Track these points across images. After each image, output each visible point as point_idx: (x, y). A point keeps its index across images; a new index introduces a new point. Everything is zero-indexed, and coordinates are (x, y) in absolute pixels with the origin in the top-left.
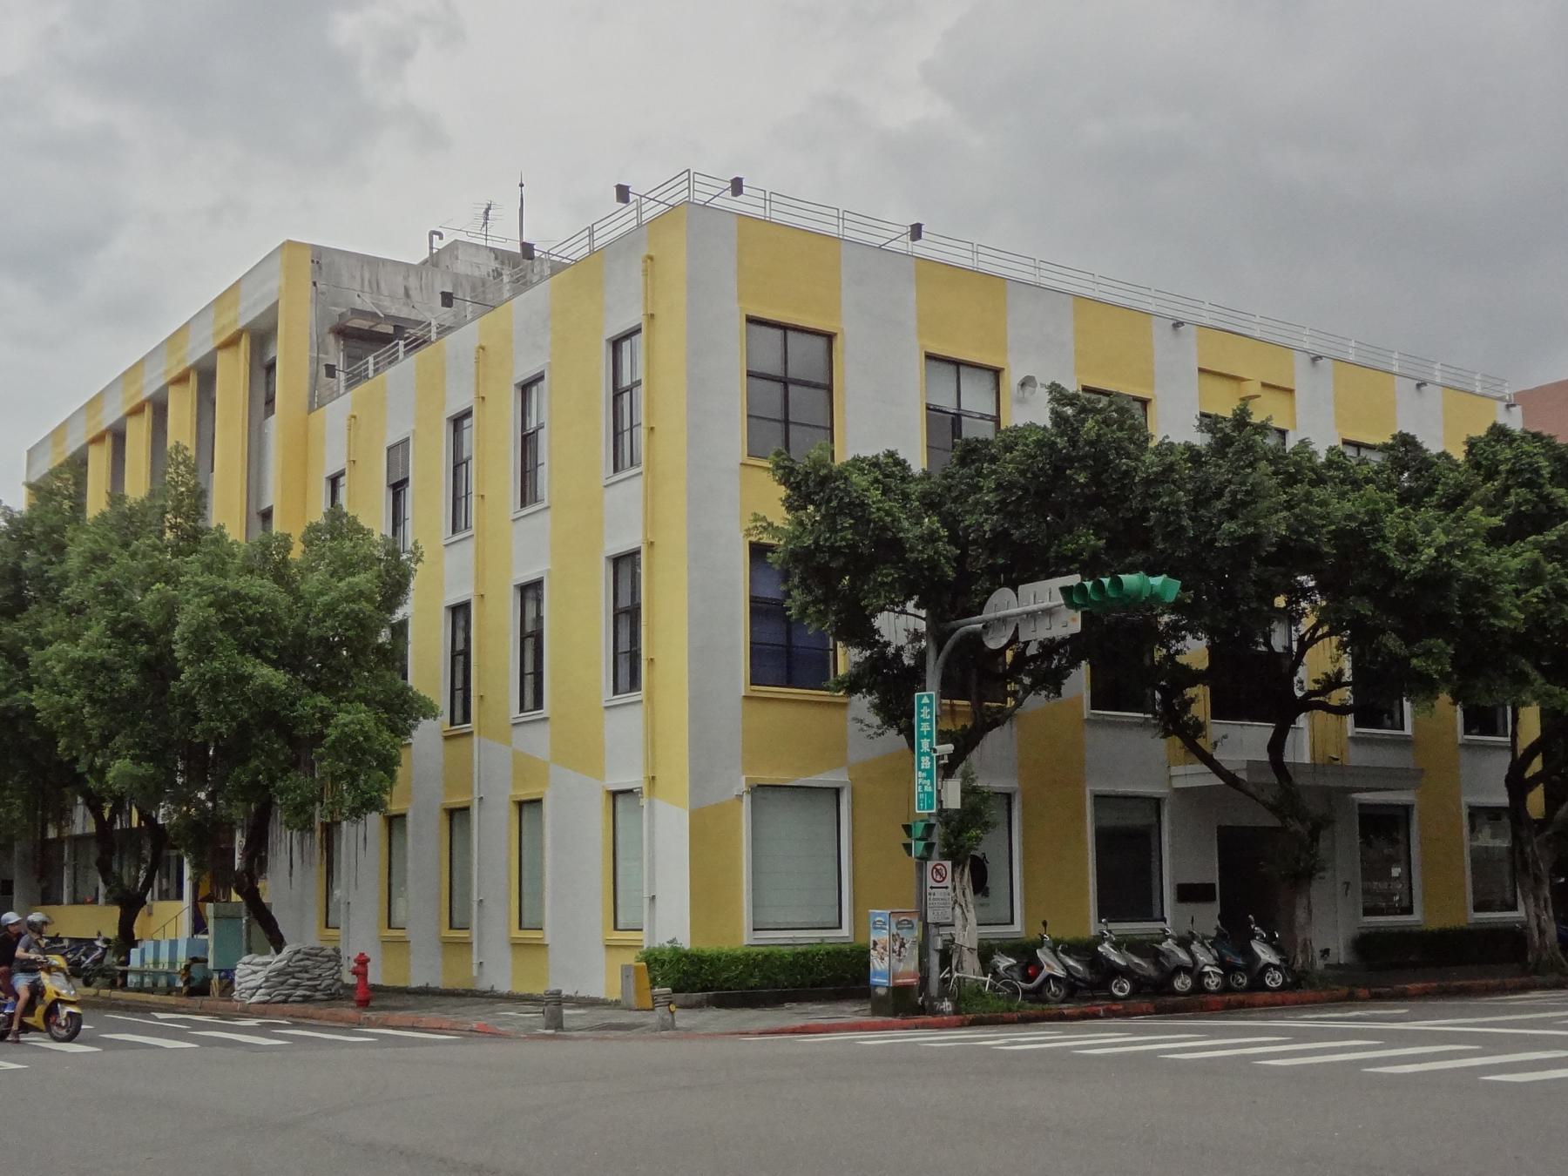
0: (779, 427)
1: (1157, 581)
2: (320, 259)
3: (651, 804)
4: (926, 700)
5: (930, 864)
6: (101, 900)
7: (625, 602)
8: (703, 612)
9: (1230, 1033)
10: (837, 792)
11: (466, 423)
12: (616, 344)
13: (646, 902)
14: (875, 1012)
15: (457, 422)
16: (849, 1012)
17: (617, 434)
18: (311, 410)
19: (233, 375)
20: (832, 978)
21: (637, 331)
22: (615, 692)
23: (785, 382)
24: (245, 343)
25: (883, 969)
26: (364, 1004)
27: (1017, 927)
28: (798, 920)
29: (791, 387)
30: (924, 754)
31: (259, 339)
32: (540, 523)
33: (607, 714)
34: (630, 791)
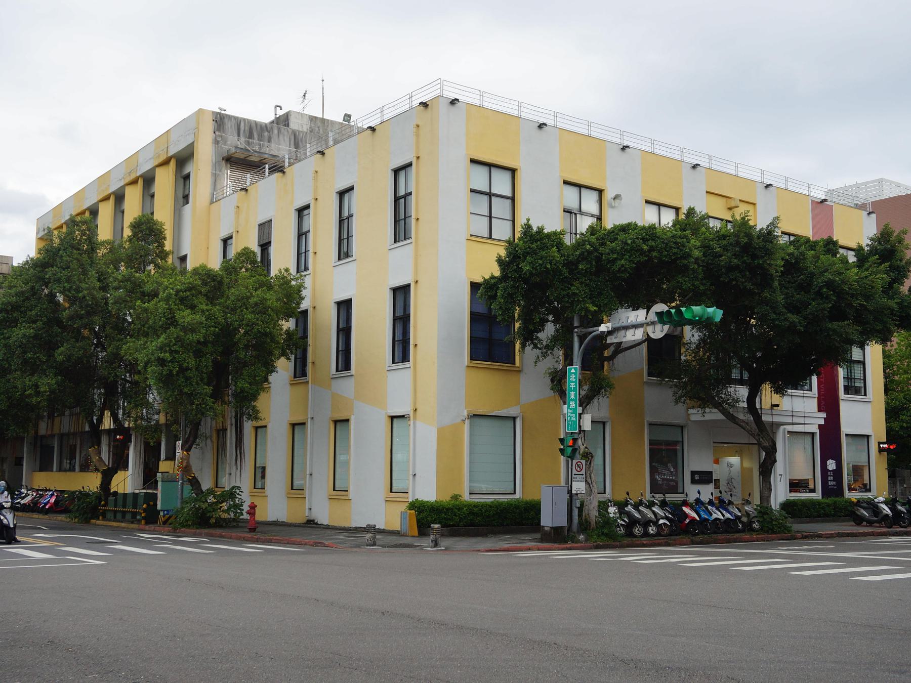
0: (486, 220)
1: (710, 310)
2: (220, 120)
3: (414, 423)
4: (573, 371)
5: (574, 462)
6: (77, 468)
7: (400, 313)
8: (444, 318)
9: (667, 553)
10: (514, 419)
11: (306, 212)
12: (396, 172)
13: (411, 477)
14: (542, 540)
15: (302, 211)
16: (526, 540)
17: (396, 222)
18: (212, 203)
19: (165, 181)
20: (509, 520)
21: (410, 165)
22: (393, 362)
23: (490, 195)
24: (173, 163)
25: (547, 520)
26: (253, 530)
27: (518, 496)
28: (497, 490)
29: (493, 198)
30: (572, 400)
31: (182, 160)
32: (349, 267)
33: (390, 374)
34: (403, 417)
